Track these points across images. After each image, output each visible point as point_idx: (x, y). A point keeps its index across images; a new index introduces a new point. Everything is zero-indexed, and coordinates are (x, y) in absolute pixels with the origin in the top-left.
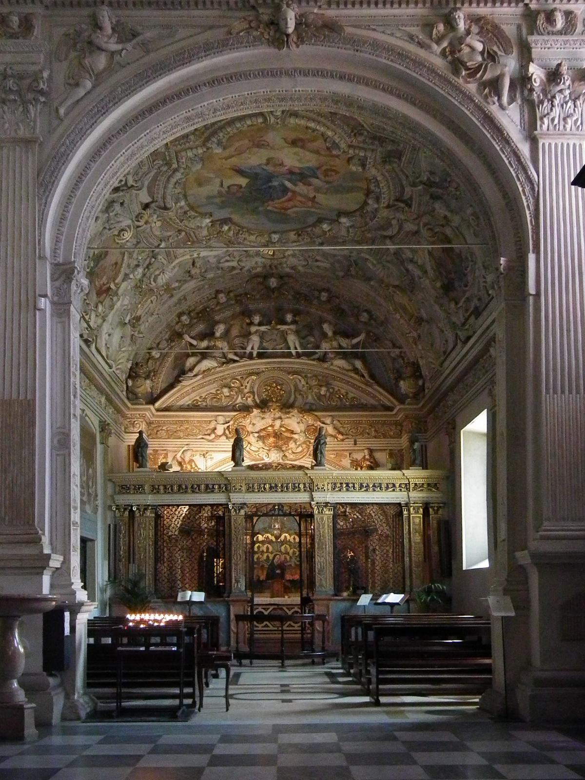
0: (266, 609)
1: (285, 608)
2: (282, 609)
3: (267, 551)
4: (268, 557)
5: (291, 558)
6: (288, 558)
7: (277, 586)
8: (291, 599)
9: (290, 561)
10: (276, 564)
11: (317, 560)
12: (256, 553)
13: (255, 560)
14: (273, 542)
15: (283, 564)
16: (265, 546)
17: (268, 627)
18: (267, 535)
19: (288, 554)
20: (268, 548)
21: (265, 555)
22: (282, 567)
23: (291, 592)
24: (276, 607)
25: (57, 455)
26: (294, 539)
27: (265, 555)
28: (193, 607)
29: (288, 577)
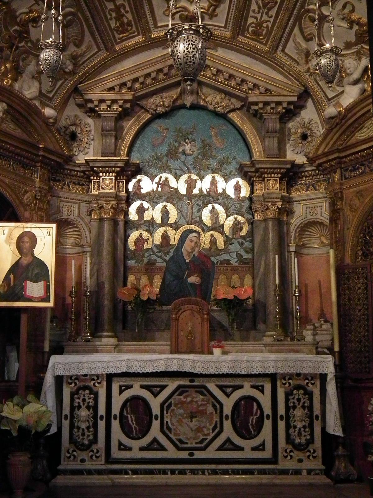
0: (155, 391)
1: (212, 386)
2: (203, 390)
3: (165, 221)
4: (165, 237)
5: (228, 241)
6: (220, 240)
7: (190, 320)
8: (229, 357)
9: (226, 250)
10: (187, 259)
11: (236, 121)
12: (136, 225)
13: (132, 247)
14: (180, 197)
15: (207, 257)
16: (160, 206)
17: (162, 448)
18: (164, 176)
19: (220, 228)
20: (165, 213)
21: (159, 232)
22: (205, 265)
23: (228, 337)
24: (185, 382)
25: (156, 27)
26: (237, 188)
27: (159, 232)
28: (16, 283)
29: (222, 290)
